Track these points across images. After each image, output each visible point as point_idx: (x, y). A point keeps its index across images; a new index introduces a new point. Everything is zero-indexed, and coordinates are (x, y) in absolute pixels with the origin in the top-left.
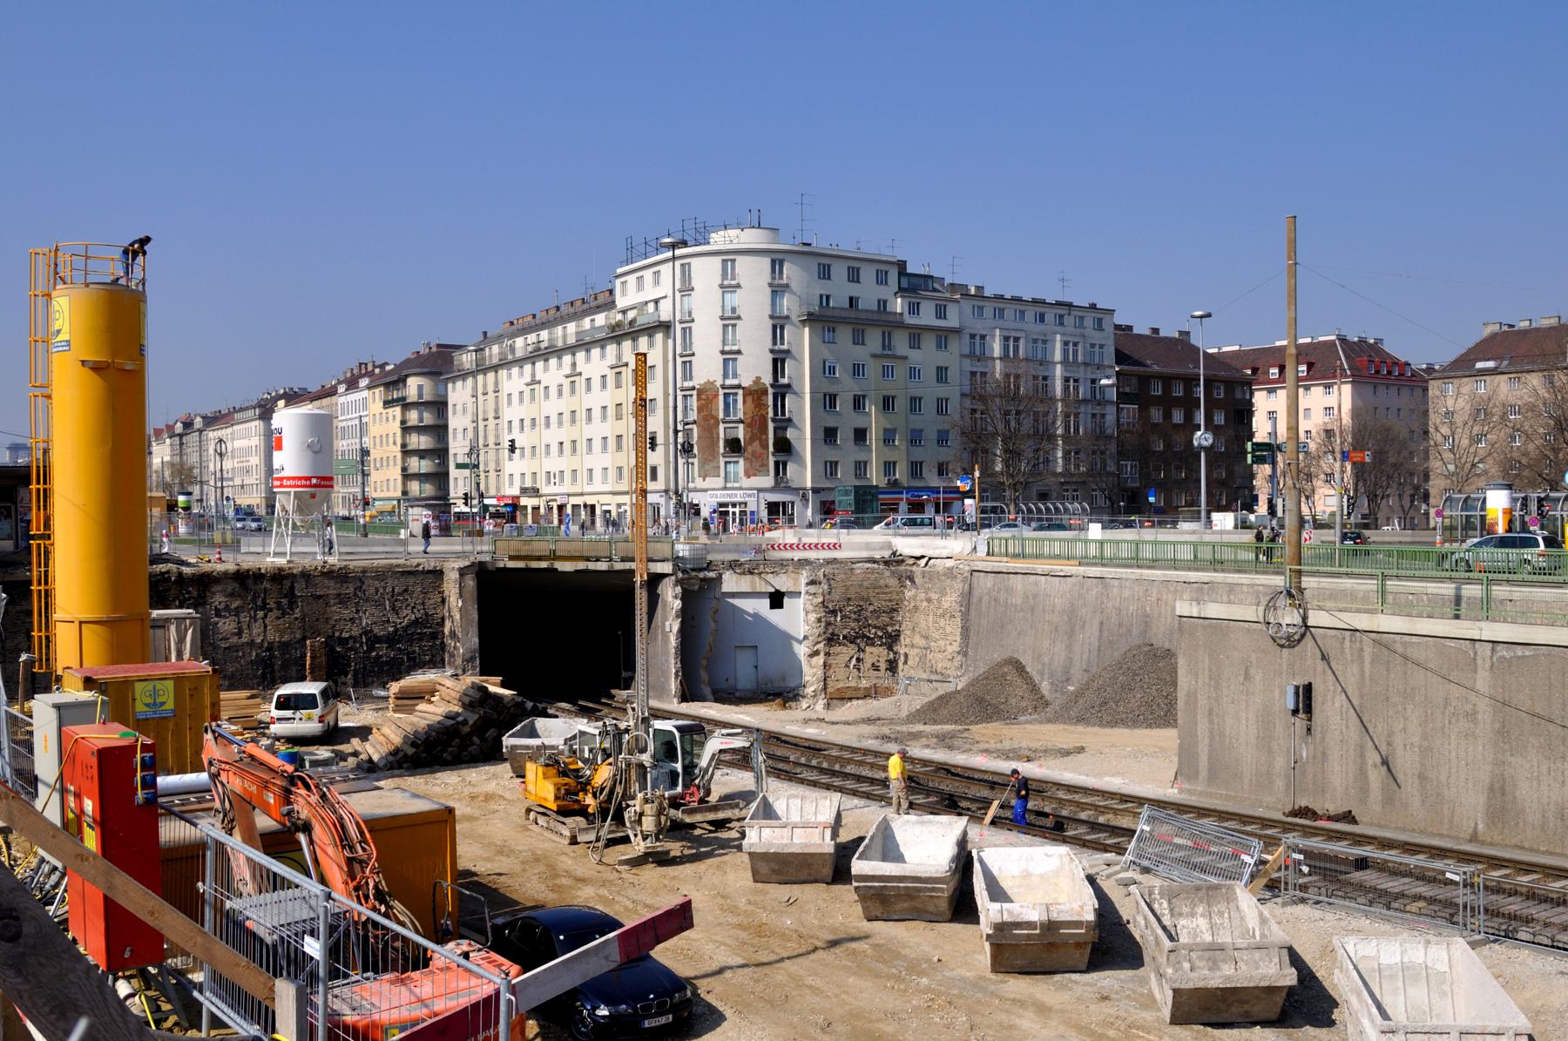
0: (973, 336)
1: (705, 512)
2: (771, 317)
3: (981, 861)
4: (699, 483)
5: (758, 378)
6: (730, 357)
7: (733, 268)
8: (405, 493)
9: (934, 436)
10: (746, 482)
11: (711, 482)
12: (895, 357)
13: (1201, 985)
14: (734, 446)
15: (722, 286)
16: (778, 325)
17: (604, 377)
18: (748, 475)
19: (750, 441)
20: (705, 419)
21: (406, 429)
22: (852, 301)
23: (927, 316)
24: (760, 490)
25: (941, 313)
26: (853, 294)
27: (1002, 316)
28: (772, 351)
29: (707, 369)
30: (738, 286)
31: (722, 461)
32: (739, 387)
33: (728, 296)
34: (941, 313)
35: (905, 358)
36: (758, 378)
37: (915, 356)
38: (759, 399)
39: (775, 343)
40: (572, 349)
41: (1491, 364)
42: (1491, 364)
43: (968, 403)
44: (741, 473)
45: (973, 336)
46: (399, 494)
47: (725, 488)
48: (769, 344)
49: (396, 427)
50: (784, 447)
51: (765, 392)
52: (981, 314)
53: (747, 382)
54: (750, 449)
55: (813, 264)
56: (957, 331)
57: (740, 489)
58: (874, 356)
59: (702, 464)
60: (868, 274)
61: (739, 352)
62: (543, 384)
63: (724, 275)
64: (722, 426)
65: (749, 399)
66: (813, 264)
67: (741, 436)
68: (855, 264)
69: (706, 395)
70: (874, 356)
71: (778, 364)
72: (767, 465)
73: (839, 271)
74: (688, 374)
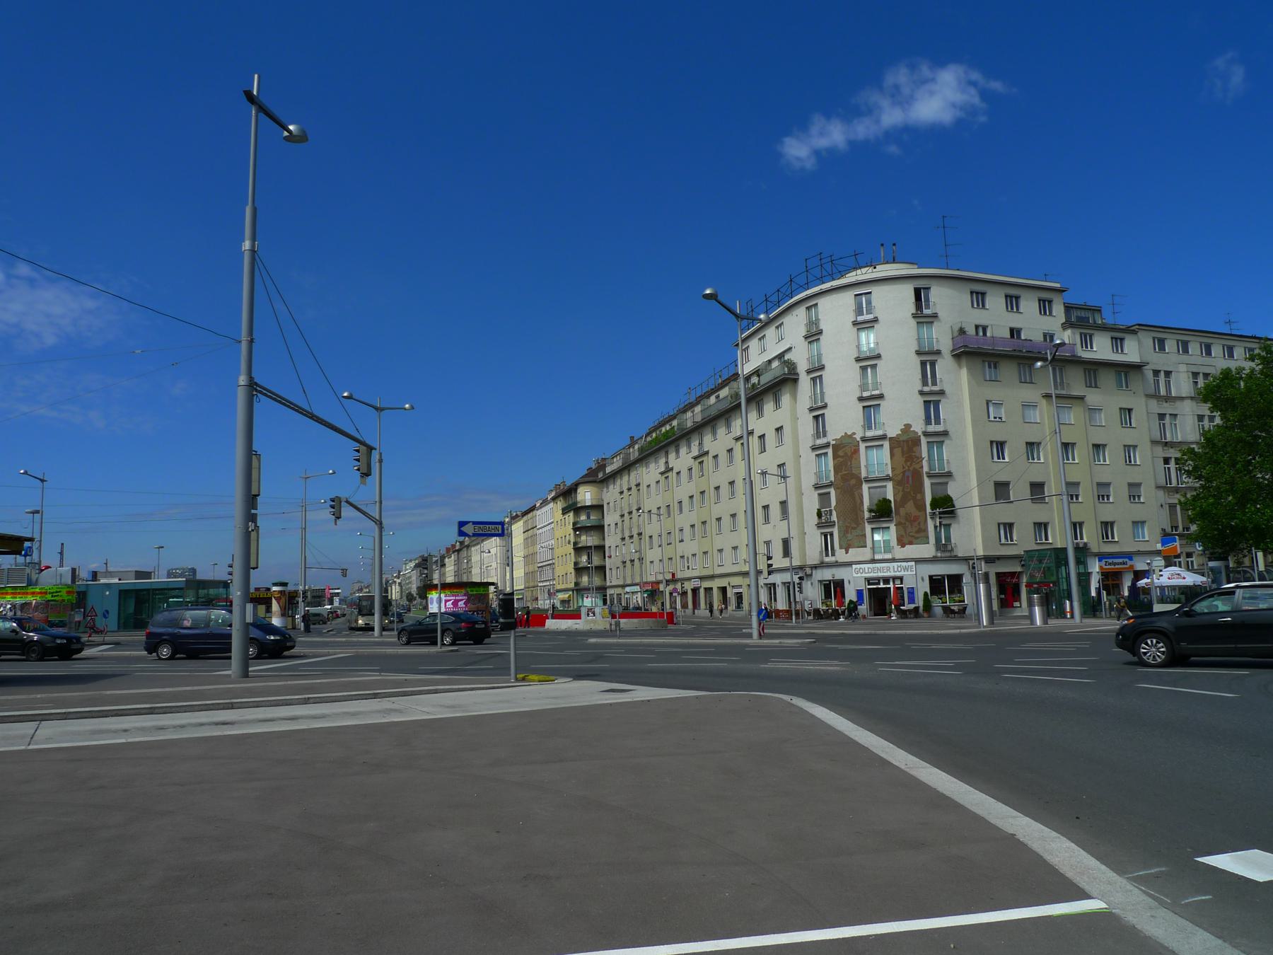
0: (1156, 373)
1: (850, 595)
2: (918, 353)
3: (648, 434)
4: (841, 556)
5: (908, 426)
6: (871, 403)
7: (869, 303)
8: (577, 584)
9: (1125, 492)
10: (900, 552)
11: (854, 555)
14: (882, 511)
15: (855, 323)
16: (928, 358)
17: (730, 451)
18: (902, 543)
19: (901, 502)
20: (845, 479)
21: (576, 528)
22: (1015, 332)
24: (918, 561)
26: (1014, 325)
27: (1186, 351)
28: (922, 393)
29: (845, 419)
30: (876, 320)
31: (868, 528)
32: (883, 437)
33: (863, 335)
35: (1082, 398)
36: (908, 426)
38: (910, 450)
39: (925, 383)
40: (698, 428)
43: (1160, 452)
44: (894, 542)
45: (1156, 373)
46: (572, 585)
47: (873, 561)
48: (918, 385)
49: (569, 529)
50: (945, 506)
51: (917, 442)
52: (1162, 348)
53: (893, 431)
54: (902, 511)
56: (1138, 367)
57: (893, 560)
59: (843, 535)
61: (881, 397)
62: (675, 471)
63: (859, 311)
64: (865, 487)
65: (898, 451)
67: (890, 496)
69: (845, 452)
71: (932, 404)
72: (926, 530)
74: (820, 429)
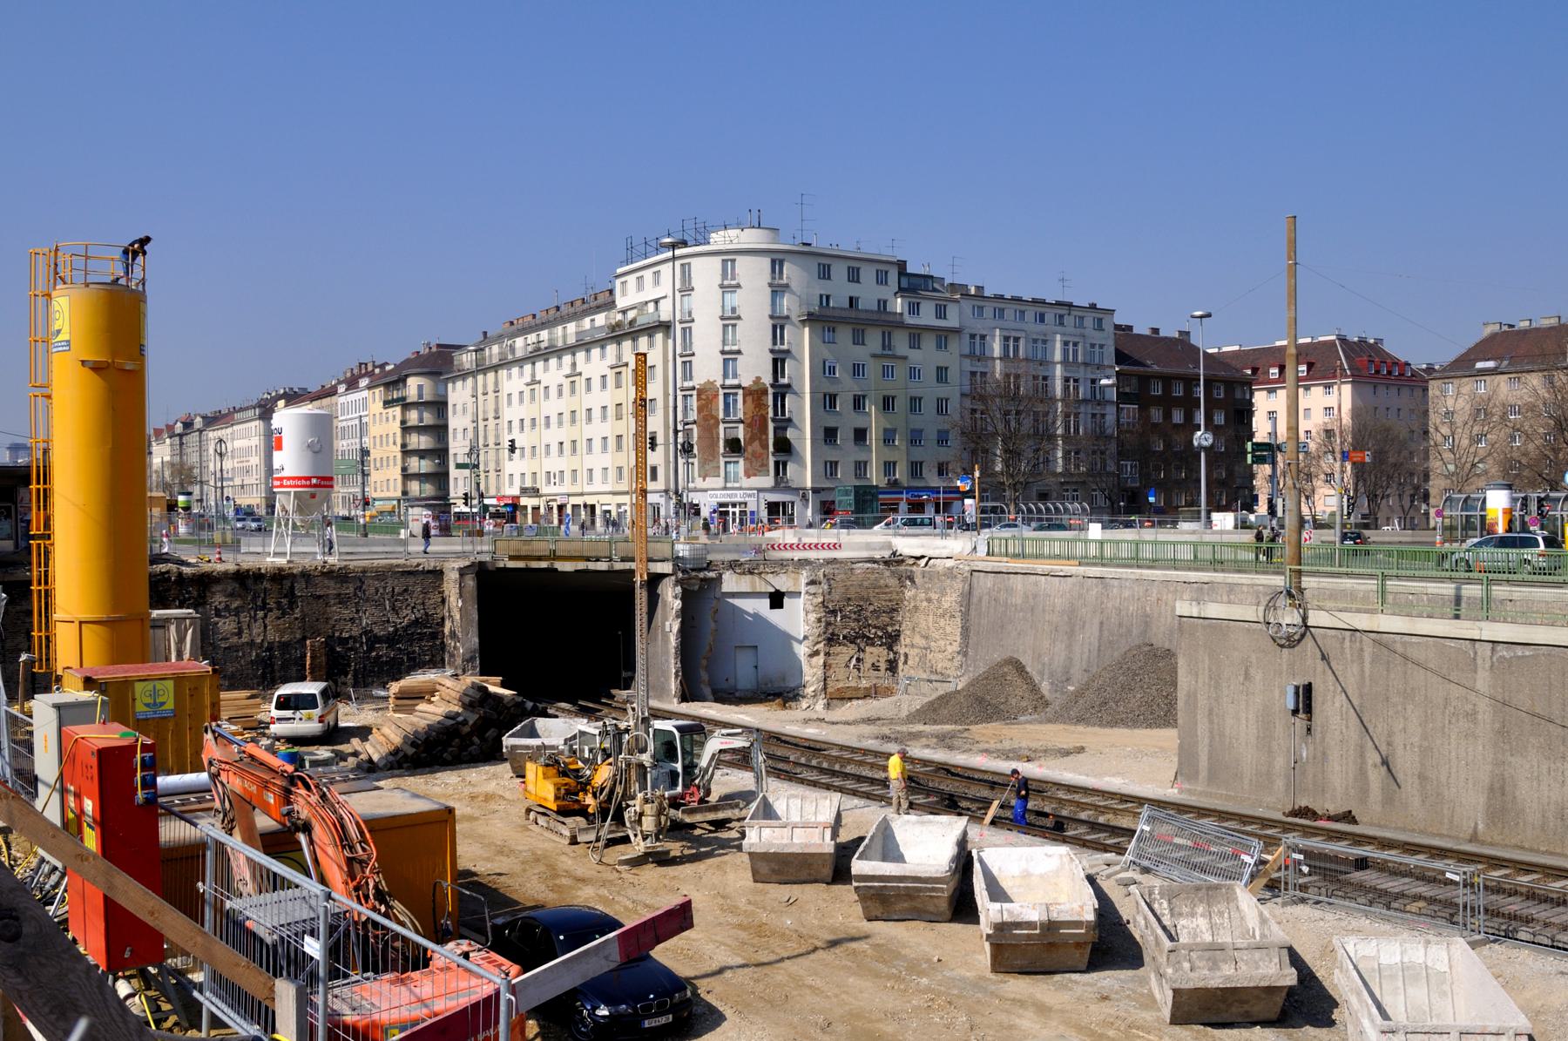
0: (973, 336)
1: (705, 512)
2: (771, 317)
3: (981, 861)
4: (699, 483)
5: (758, 378)
6: (730, 357)
7: (733, 268)
8: (405, 493)
9: (934, 436)
10: (746, 482)
11: (711, 482)
12: (895, 357)
13: (1201, 985)
14: (734, 446)
15: (722, 286)
16: (778, 325)
17: (604, 377)
18: (748, 475)
19: (750, 441)
20: (705, 419)
21: (406, 429)
22: (852, 301)
23: (927, 316)
24: (760, 490)
25: (941, 313)
26: (853, 294)
27: (1002, 316)
28: (772, 351)
29: (707, 369)
30: (738, 286)
31: (722, 461)
32: (739, 387)
33: (728, 296)
34: (941, 313)
35: (905, 358)
36: (758, 378)
37: (915, 356)
38: (759, 399)
39: (775, 343)
40: (572, 349)
41: (1491, 364)
42: (1491, 364)
43: (968, 403)
44: (741, 473)
45: (973, 336)
46: (399, 494)
47: (725, 488)
48: (769, 344)
49: (396, 427)
50: (784, 447)
51: (765, 392)
52: (981, 314)
53: (747, 382)
54: (750, 449)
55: (813, 264)
56: (957, 331)
57: (740, 489)
58: (874, 356)
59: (702, 464)
60: (868, 274)
61: (739, 352)
62: (543, 384)
63: (724, 275)
64: (722, 426)
65: (749, 399)
66: (813, 264)
67: (741, 436)
68: (855, 264)
69: (706, 395)
70: (874, 356)
71: (778, 364)
72: (767, 465)
73: (839, 271)
74: (688, 374)
